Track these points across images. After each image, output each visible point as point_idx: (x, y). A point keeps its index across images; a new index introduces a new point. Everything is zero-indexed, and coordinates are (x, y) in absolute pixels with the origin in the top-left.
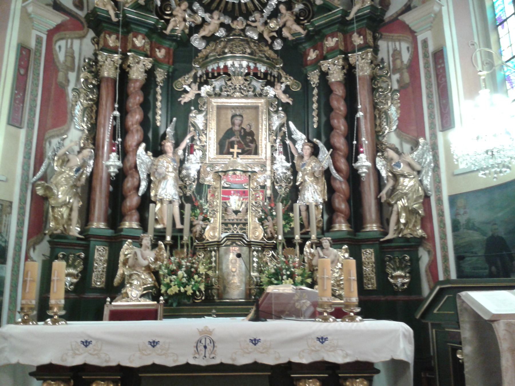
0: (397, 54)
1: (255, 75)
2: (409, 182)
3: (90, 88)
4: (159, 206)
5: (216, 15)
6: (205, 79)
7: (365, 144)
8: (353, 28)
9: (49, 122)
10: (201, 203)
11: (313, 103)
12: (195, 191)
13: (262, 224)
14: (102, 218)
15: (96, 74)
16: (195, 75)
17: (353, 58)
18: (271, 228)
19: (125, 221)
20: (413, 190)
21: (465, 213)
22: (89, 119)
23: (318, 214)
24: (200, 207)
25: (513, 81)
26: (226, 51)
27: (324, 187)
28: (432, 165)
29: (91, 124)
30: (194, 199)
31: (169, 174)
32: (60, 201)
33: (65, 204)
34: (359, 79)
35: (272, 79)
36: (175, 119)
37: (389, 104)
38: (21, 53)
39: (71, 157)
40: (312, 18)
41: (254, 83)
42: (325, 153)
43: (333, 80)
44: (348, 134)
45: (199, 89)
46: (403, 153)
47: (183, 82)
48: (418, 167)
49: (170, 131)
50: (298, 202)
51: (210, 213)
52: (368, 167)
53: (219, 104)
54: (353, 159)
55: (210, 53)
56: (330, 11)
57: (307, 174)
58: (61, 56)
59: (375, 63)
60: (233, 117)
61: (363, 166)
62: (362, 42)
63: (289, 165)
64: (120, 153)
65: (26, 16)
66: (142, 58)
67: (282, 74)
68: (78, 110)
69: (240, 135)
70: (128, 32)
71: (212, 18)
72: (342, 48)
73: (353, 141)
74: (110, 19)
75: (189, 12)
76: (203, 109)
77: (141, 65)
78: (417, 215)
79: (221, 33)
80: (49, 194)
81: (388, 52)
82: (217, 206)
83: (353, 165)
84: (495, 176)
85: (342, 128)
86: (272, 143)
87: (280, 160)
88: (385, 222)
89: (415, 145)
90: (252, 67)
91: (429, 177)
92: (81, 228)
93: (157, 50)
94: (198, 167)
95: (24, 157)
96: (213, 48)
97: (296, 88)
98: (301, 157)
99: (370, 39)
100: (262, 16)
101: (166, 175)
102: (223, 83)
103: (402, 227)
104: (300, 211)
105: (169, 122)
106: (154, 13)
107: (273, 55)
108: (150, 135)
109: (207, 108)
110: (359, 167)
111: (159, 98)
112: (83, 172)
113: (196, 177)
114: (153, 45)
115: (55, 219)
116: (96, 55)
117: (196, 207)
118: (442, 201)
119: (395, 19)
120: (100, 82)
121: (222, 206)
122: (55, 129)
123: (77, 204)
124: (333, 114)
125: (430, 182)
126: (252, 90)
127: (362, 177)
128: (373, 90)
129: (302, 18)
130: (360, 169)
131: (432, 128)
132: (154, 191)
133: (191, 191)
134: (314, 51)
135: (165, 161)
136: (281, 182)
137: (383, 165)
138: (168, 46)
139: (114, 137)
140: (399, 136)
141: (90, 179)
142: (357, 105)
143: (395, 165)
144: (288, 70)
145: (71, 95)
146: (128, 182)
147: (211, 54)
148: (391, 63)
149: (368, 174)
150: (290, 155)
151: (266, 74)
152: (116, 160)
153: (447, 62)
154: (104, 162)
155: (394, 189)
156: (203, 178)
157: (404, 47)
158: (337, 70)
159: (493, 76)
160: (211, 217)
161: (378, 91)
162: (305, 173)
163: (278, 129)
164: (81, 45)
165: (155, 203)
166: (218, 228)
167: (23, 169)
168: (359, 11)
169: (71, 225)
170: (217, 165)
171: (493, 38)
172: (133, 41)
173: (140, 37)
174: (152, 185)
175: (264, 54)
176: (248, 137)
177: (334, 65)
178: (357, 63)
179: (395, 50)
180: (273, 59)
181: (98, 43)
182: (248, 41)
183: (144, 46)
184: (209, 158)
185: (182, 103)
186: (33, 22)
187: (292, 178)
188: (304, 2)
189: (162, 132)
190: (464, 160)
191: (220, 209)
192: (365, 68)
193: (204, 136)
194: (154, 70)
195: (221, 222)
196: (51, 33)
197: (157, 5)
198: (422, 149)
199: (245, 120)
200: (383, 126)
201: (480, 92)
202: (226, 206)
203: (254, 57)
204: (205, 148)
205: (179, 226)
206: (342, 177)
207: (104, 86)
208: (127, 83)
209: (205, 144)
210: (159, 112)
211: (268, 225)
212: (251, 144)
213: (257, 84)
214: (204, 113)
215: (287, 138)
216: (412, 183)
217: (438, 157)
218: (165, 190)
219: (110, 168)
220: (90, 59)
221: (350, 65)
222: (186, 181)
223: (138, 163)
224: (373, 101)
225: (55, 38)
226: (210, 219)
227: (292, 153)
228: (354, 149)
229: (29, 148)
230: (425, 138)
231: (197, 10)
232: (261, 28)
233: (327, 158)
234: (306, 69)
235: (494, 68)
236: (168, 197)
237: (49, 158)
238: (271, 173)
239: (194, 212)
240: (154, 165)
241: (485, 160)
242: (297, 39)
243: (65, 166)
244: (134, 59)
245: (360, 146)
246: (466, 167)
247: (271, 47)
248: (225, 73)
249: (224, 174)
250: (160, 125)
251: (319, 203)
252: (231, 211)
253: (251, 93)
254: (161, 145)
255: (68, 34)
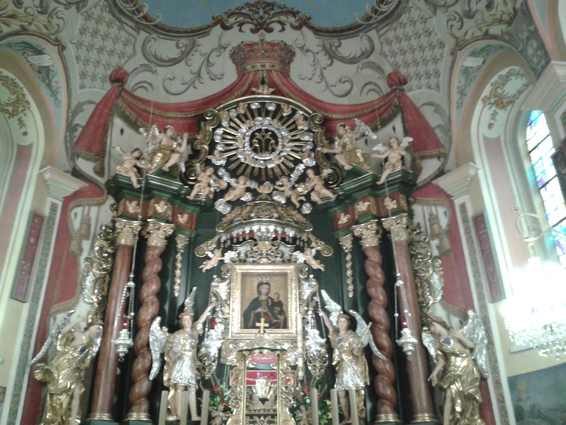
0: (434, 219)
1: (283, 240)
2: (462, 361)
3: (104, 257)
4: (172, 392)
5: (242, 180)
6: (229, 244)
7: (409, 317)
8: (385, 192)
9: (57, 294)
10: (222, 389)
11: (347, 269)
12: (215, 373)
13: (294, 416)
14: (106, 408)
15: (113, 243)
16: (219, 240)
17: (387, 223)
18: (304, 420)
19: (133, 411)
20: (467, 371)
21: (528, 398)
22: (101, 291)
23: (360, 401)
24: (220, 393)
25: (563, 246)
26: (252, 215)
27: (365, 368)
28: (486, 341)
29: (102, 296)
30: (213, 383)
31: (187, 353)
32: (60, 387)
33: (66, 391)
34: (396, 244)
35: (302, 244)
36: (195, 288)
37: (431, 272)
38: (33, 222)
39: (76, 334)
40: (341, 183)
41: (282, 248)
42: (364, 327)
43: (367, 245)
44: (388, 305)
45: (223, 255)
46: (452, 327)
47: (205, 248)
48: (470, 344)
49: (189, 302)
50: (335, 386)
51: (232, 402)
52: (414, 345)
53: (244, 271)
54: (397, 334)
55: (235, 218)
56: (360, 176)
57: (344, 352)
58: (76, 224)
59: (411, 228)
60: (260, 285)
61: (408, 343)
62: (395, 206)
63: (323, 341)
64: (132, 329)
65: (42, 184)
66: (163, 224)
67: (312, 239)
68: (89, 282)
69: (267, 305)
70: (149, 199)
71: (237, 182)
72: (374, 212)
73: (394, 313)
74: (131, 185)
75: (214, 177)
76: (227, 277)
77: (161, 231)
78: (474, 402)
79: (247, 197)
80: (48, 379)
81: (424, 216)
82: (240, 392)
83: (397, 341)
84: (558, 354)
85: (381, 297)
86: (303, 315)
87: (312, 335)
88: (439, 411)
89: (464, 319)
90: (280, 232)
91: (483, 356)
92: (81, 420)
93: (179, 216)
94: (219, 344)
95: (25, 336)
96: (238, 213)
97: (328, 254)
98: (337, 331)
99: (403, 203)
100: (290, 181)
101: (184, 354)
102: (249, 248)
103: (458, 416)
104: (338, 397)
105: (188, 292)
106: (178, 179)
107: (302, 219)
108: (167, 307)
109: (230, 276)
110: (403, 344)
111: (179, 265)
112: (88, 351)
113: (217, 356)
114: (176, 210)
115: (53, 409)
116: (114, 222)
117: (215, 394)
118: (501, 384)
119: (428, 183)
120: (116, 250)
121: (247, 393)
122: (61, 303)
123: (79, 390)
124: (369, 282)
125: (485, 362)
126: (280, 255)
127: (408, 356)
128: (412, 257)
129: (331, 182)
130: (405, 347)
131: (481, 299)
132: (167, 374)
133: (211, 374)
134: (345, 215)
135: (182, 338)
136: (315, 361)
137: (431, 342)
138: (191, 211)
139: (126, 311)
140: (445, 307)
141: (96, 360)
142: (396, 273)
143: (444, 342)
144: (319, 234)
145: (83, 264)
146: (138, 363)
147: (236, 219)
148: (428, 228)
149: (414, 352)
150: (324, 330)
151: (294, 239)
152: (126, 338)
153: (490, 228)
154: (112, 341)
155: (445, 370)
156: (225, 357)
157: (441, 212)
158: (371, 235)
159: (541, 242)
160: (234, 407)
161: (416, 258)
162: (342, 350)
163: (310, 299)
164: (99, 211)
165: (167, 389)
166: (242, 420)
167: (22, 349)
168: (390, 175)
169: (70, 416)
170: (241, 340)
171: (536, 202)
172: (154, 208)
173: (162, 203)
174: (165, 368)
175: (292, 218)
176: (276, 308)
177: (368, 229)
178: (392, 228)
179: (431, 215)
180: (303, 223)
181: (117, 210)
182: (276, 205)
183: (166, 212)
184: (232, 332)
185: (204, 270)
186: (48, 189)
187: (327, 356)
188: (333, 167)
189: (180, 304)
190: (520, 337)
191: (244, 397)
192: (401, 234)
193: (227, 307)
194: (175, 237)
195: (245, 414)
196: (67, 201)
197: (181, 172)
198: (472, 323)
199: (272, 288)
200: (426, 296)
201: (529, 260)
202: (251, 393)
203: (281, 221)
204: (227, 321)
205: (195, 418)
206: (384, 355)
207: (120, 255)
208: (145, 250)
209: (228, 316)
210: (178, 281)
211: (301, 417)
212: (279, 316)
213: (286, 249)
214: (228, 281)
215: (320, 309)
216: (465, 363)
217: (491, 332)
218: (180, 373)
219: (119, 348)
220: (107, 227)
221: (384, 230)
222: (205, 361)
223: (151, 340)
224: (413, 268)
225: (72, 204)
226: (232, 409)
227: (326, 327)
228: (396, 322)
229: (31, 324)
230: (474, 310)
231: (223, 175)
232: (288, 193)
233: (366, 332)
234: (337, 234)
235: (542, 234)
236: (183, 382)
237: (52, 337)
238: (303, 351)
239: (214, 400)
240: (169, 342)
241: (543, 336)
242: (326, 204)
243: (68, 345)
244: (154, 226)
245: (402, 319)
246: (524, 345)
247: (299, 210)
248: (250, 238)
249: (248, 353)
250: (179, 295)
251: (360, 388)
252: (257, 399)
253: (279, 259)
254: (178, 319)
255: (85, 200)
